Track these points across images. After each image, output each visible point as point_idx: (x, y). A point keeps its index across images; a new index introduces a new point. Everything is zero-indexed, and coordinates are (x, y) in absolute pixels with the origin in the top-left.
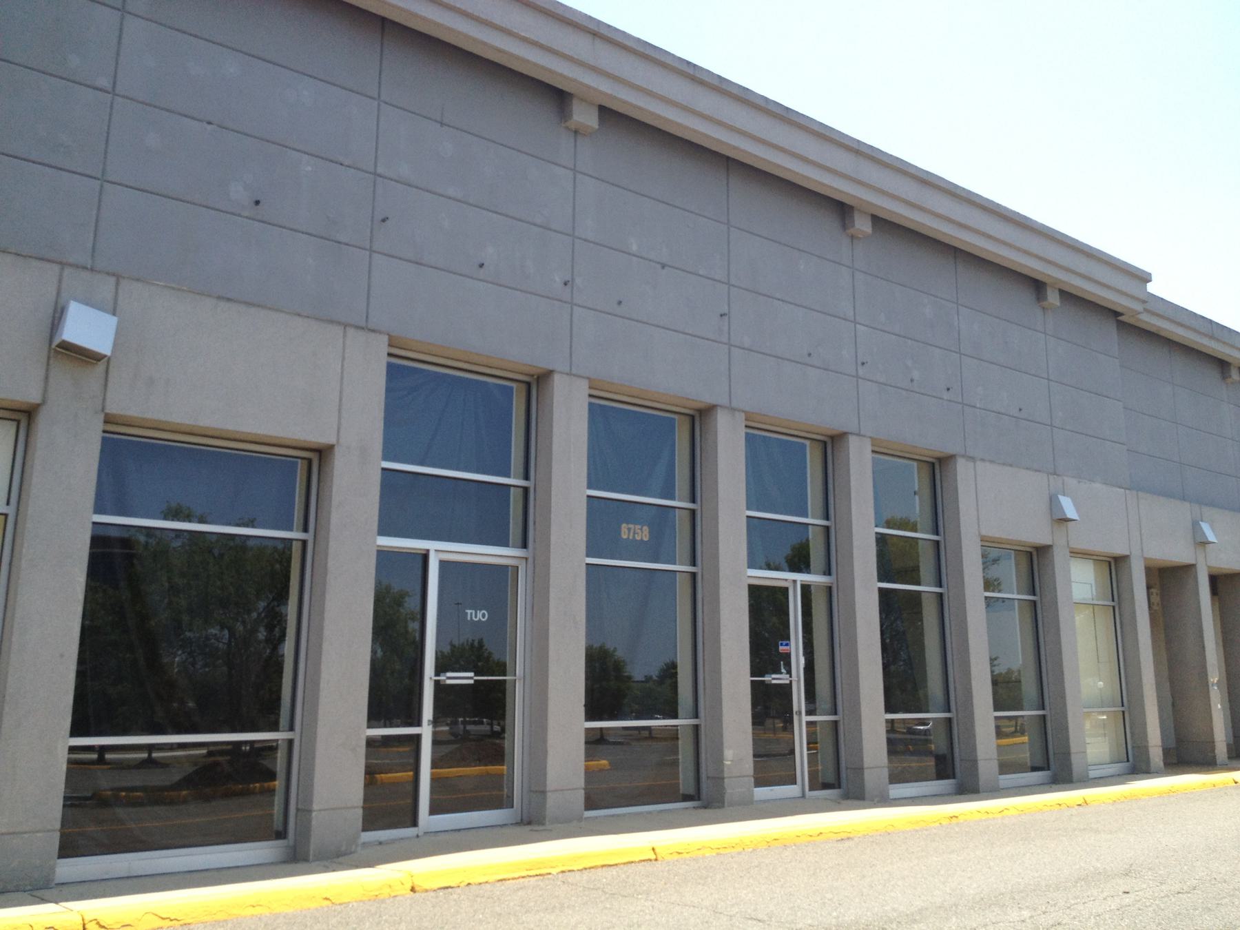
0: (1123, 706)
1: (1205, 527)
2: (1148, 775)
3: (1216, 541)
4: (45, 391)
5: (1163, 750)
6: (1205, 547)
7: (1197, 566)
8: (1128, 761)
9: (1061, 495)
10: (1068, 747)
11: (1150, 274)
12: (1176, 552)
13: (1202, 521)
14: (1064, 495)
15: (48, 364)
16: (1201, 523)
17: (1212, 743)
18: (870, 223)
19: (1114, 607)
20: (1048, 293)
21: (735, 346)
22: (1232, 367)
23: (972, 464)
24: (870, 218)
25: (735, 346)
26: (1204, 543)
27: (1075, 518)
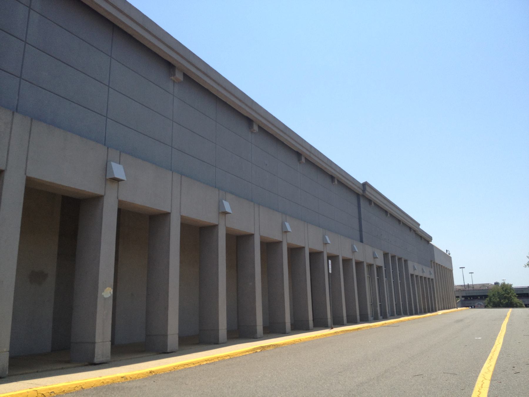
0: (372, 302)
1: (287, 224)
2: (285, 334)
3: (231, 213)
4: (105, 192)
5: (179, 337)
6: (225, 215)
7: (255, 235)
8: (373, 317)
9: (224, 200)
10: (343, 316)
11: (432, 237)
12: (275, 235)
13: (286, 222)
14: (225, 201)
15: (219, 217)
16: (224, 201)
17: (308, 321)
18: (182, 77)
19: (369, 277)
20: (176, 73)
21: (23, 79)
22: (254, 124)
23: (465, 284)
24: (183, 74)
25: (23, 79)
26: (326, 244)
27: (124, 179)
